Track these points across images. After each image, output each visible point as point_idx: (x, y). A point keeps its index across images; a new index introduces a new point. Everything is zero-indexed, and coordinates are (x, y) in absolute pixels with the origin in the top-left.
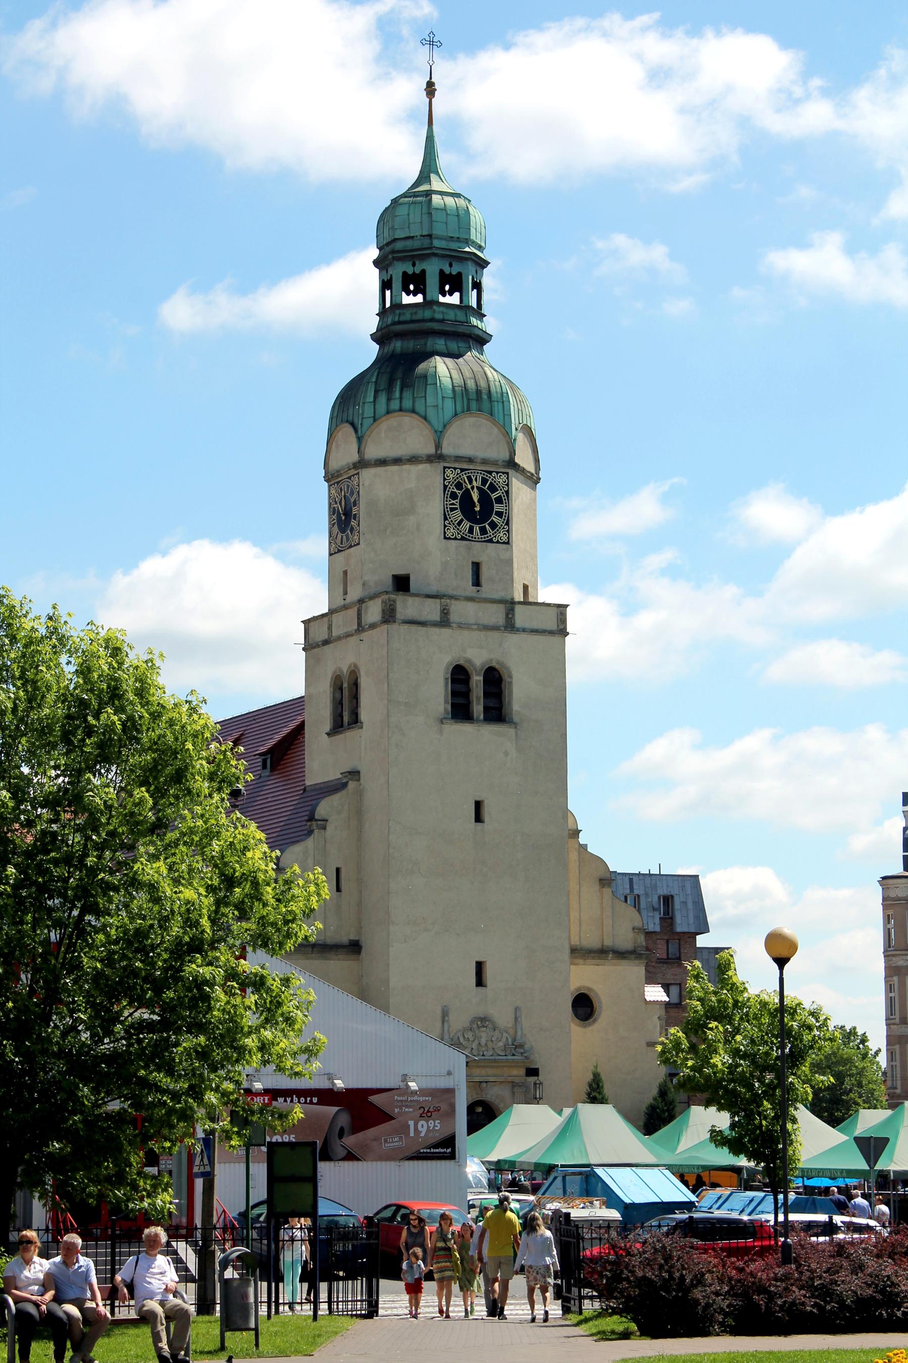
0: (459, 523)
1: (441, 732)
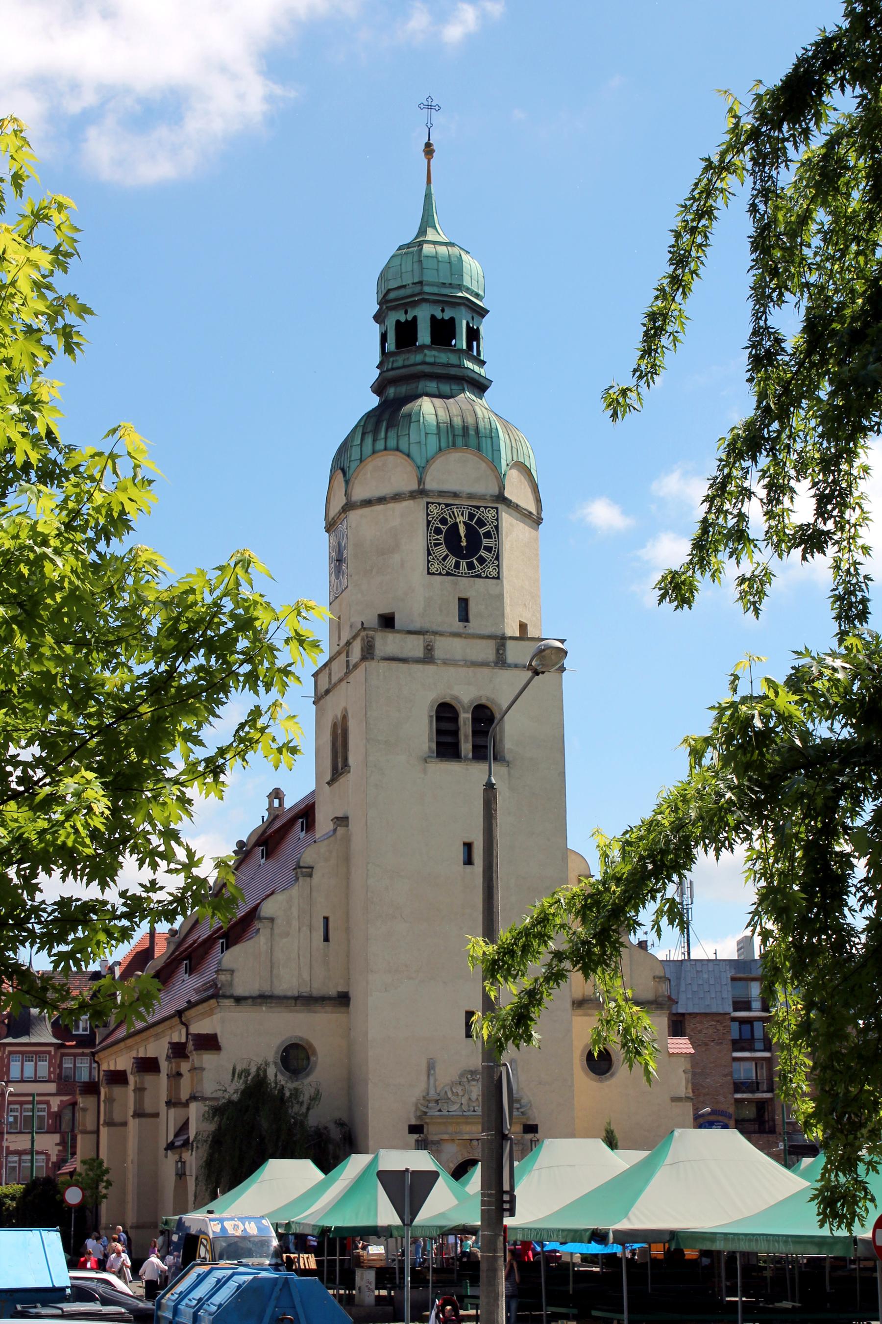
0: (444, 559)
1: (425, 771)
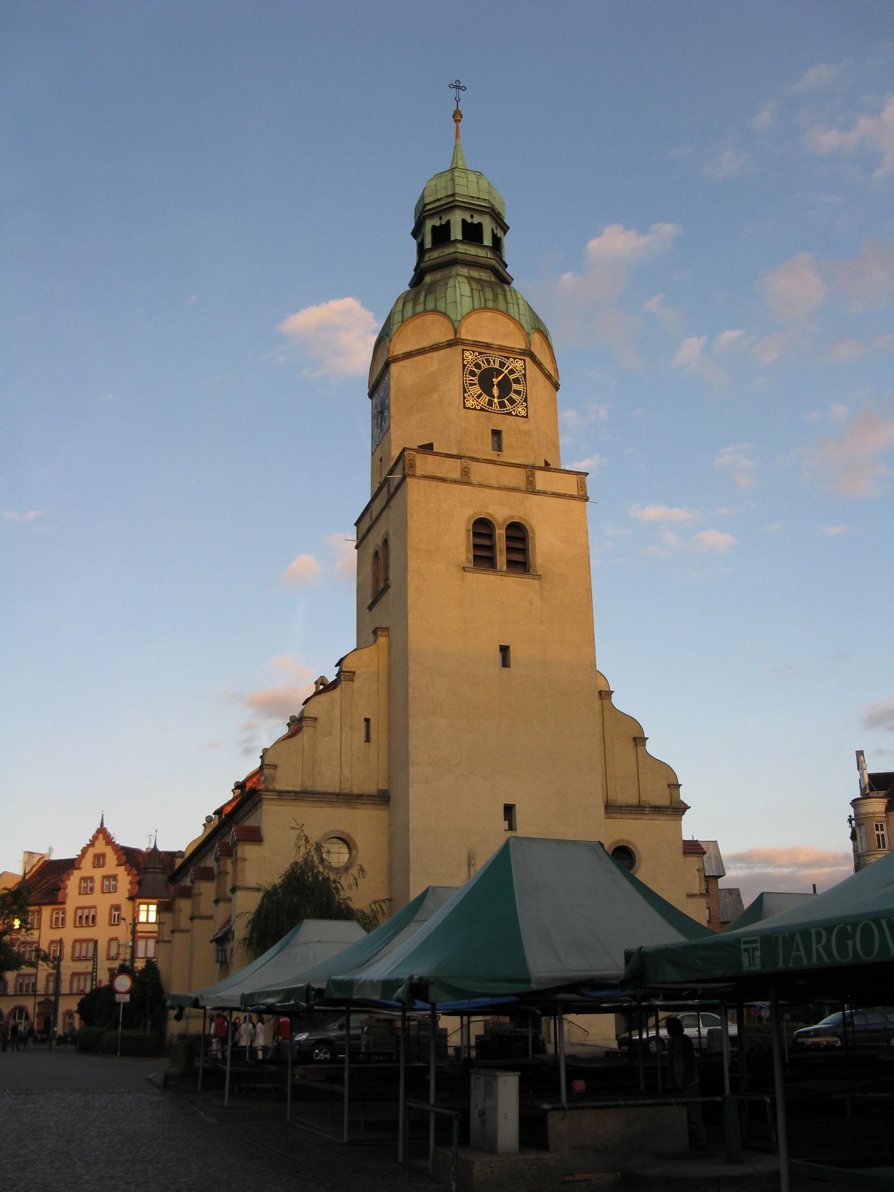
0: (479, 396)
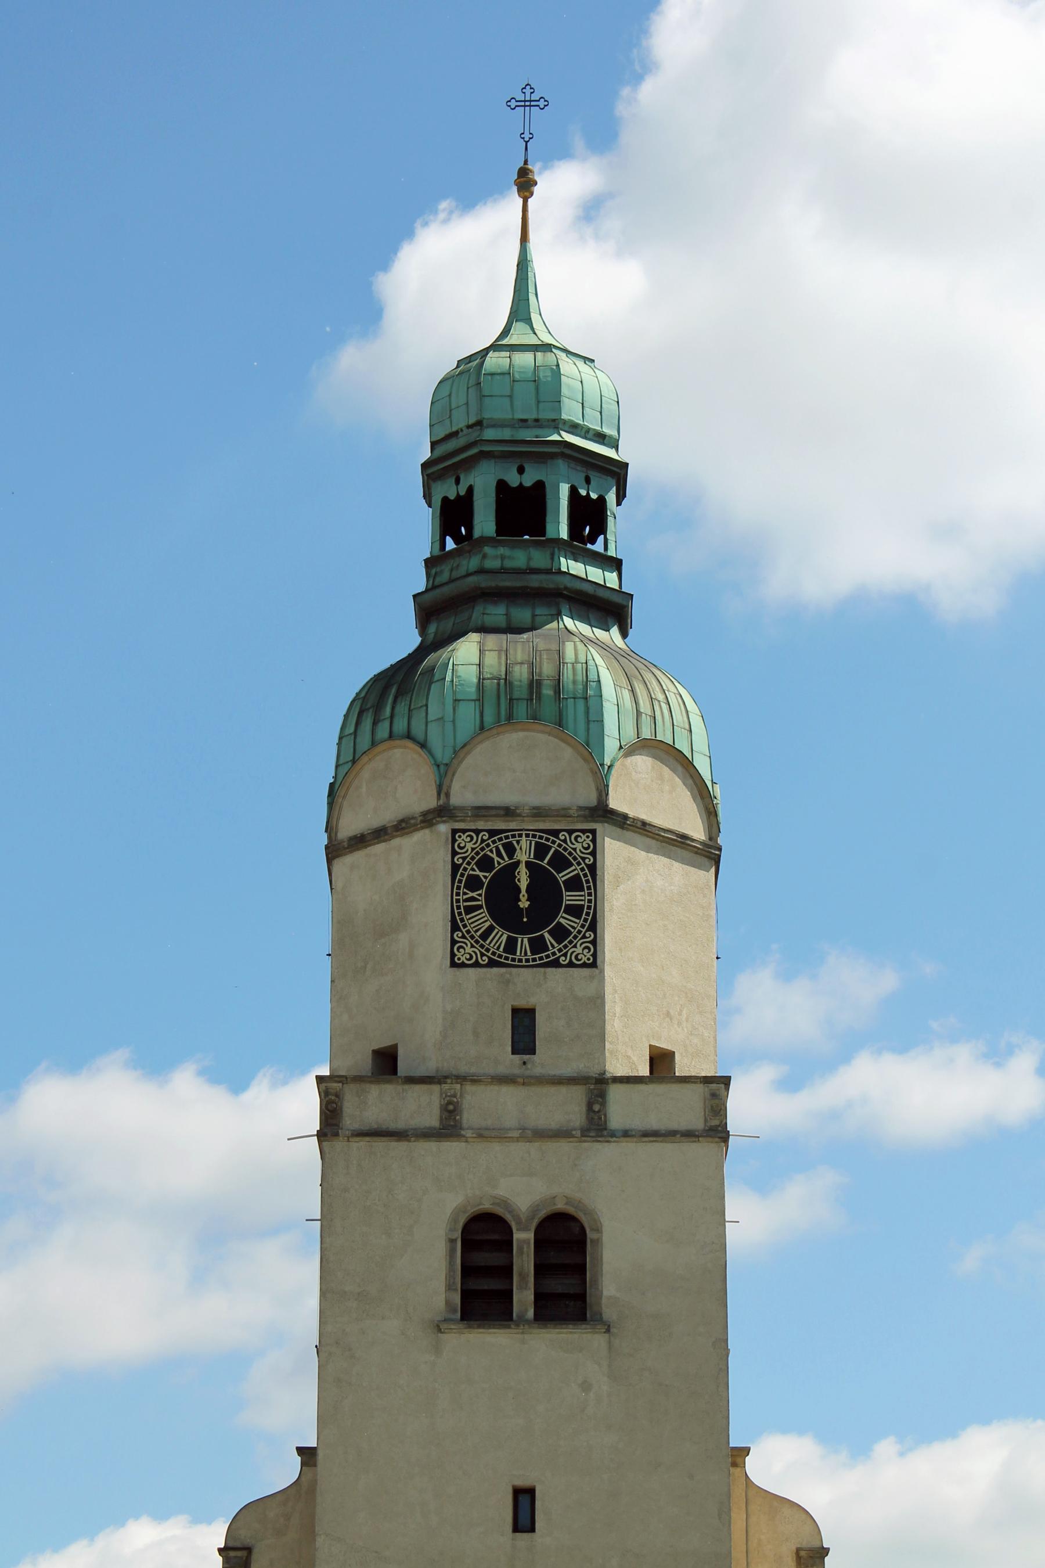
0: (485, 936)
1: (437, 1350)
